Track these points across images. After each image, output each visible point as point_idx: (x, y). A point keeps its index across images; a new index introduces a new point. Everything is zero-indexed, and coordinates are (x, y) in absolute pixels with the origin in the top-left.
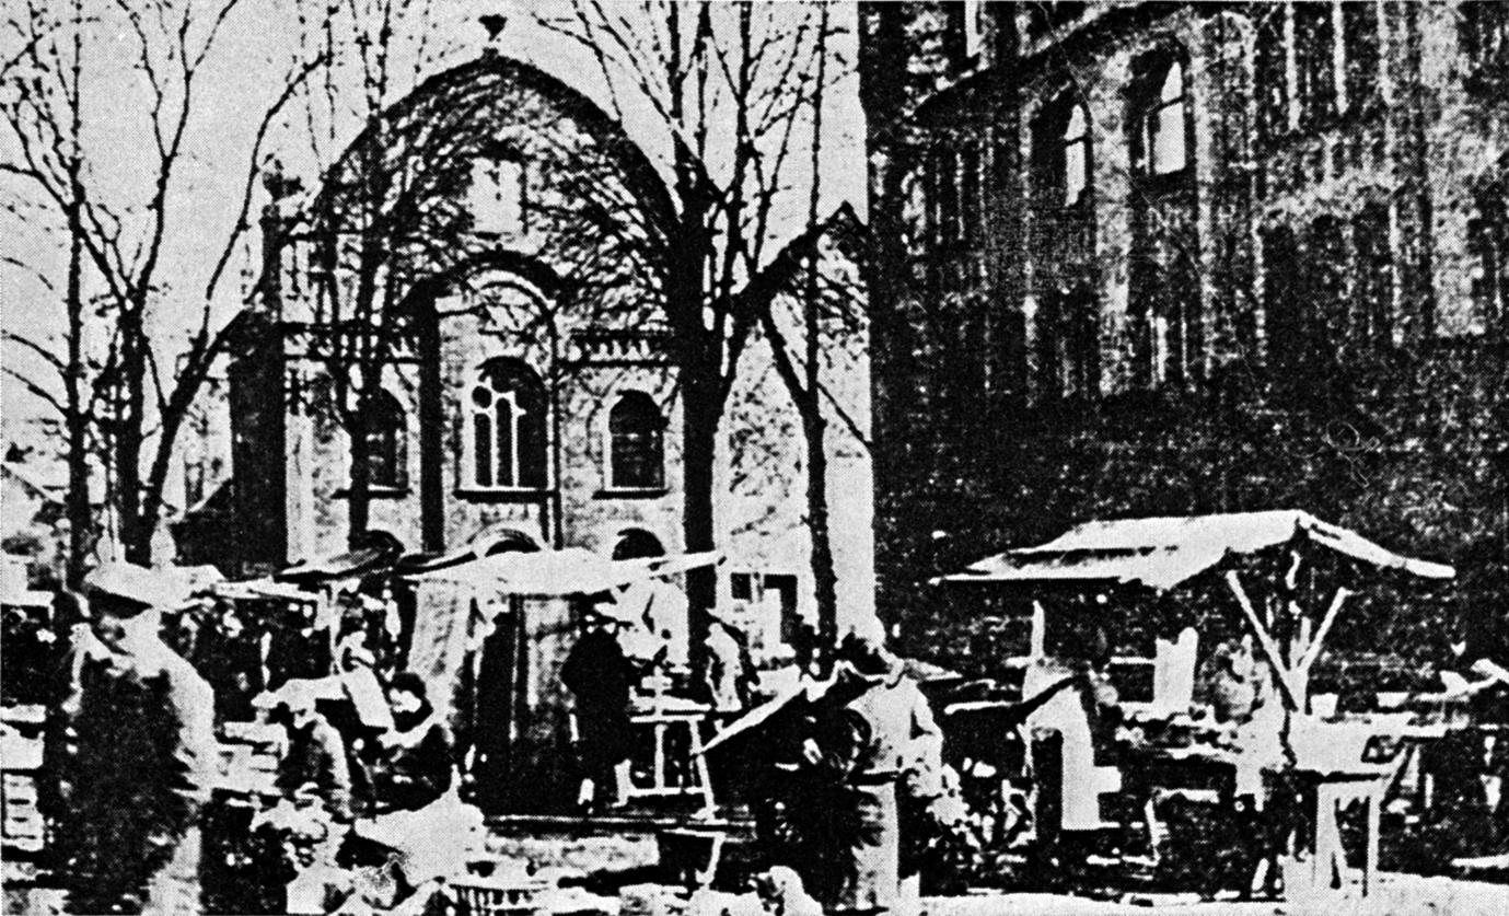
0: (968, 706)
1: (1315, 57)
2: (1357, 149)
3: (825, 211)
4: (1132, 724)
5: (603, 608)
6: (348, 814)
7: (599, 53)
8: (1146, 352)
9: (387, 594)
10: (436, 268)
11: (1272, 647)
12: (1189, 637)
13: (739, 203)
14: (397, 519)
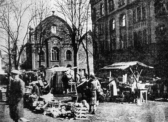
0: (103, 82)
1: (139, 14)
2: (143, 24)
3: (88, 31)
4: (120, 84)
5: (66, 73)
6: (39, 95)
7: (64, 15)
8: (121, 46)
9: (43, 72)
10: (48, 37)
11: (135, 76)
12: (126, 75)
13: (79, 30)
14: (44, 64)
